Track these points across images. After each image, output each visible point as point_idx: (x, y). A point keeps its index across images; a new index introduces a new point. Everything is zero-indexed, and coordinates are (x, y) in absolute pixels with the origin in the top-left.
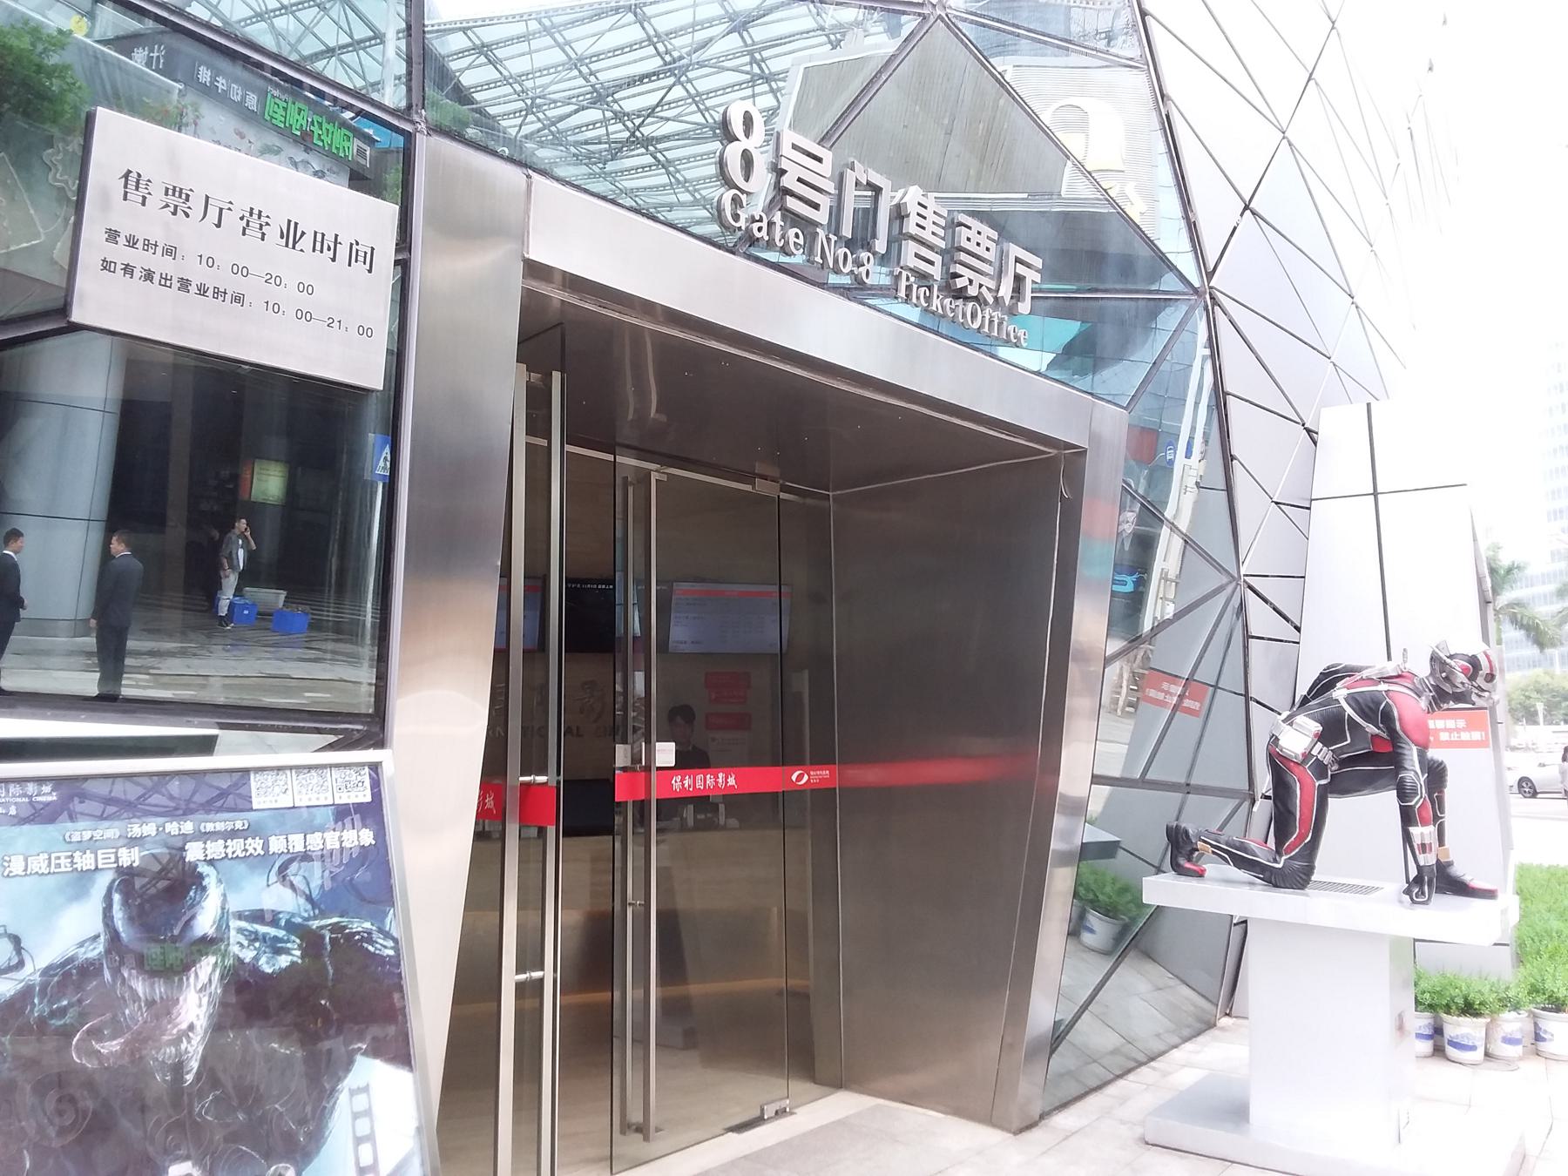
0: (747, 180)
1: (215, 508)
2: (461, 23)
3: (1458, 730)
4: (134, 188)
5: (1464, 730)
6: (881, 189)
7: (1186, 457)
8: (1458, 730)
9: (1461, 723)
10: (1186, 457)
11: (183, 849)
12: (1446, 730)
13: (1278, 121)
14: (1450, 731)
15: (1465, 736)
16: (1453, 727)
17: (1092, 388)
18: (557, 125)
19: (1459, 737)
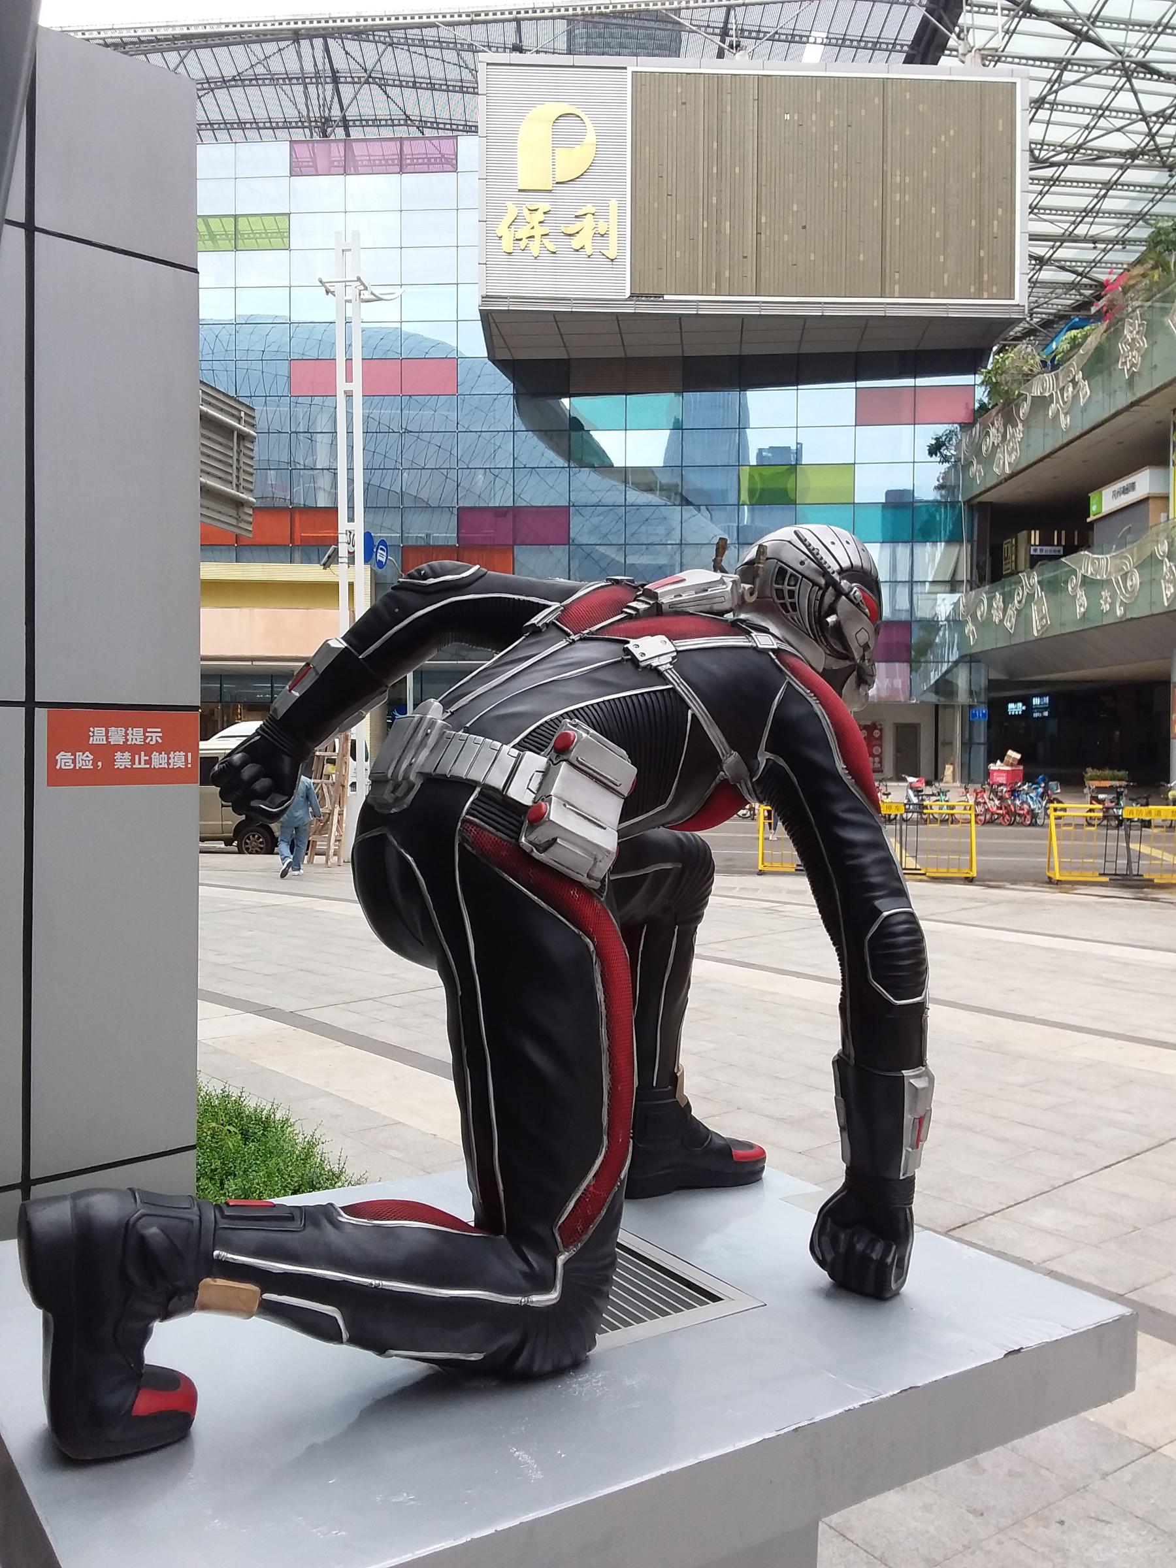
0: (795, 532)
1: (921, 634)
2: (242, 26)
3: (148, 749)
4: (838, 29)
5: (159, 748)
6: (760, 449)
7: (355, 740)
8: (148, 749)
9: (155, 736)
10: (355, 740)
11: (951, 764)
12: (124, 748)
13: (798, 651)
14: (134, 750)
15: (159, 760)
16: (139, 742)
17: (206, 248)
18: (621, 501)
19: (149, 762)
